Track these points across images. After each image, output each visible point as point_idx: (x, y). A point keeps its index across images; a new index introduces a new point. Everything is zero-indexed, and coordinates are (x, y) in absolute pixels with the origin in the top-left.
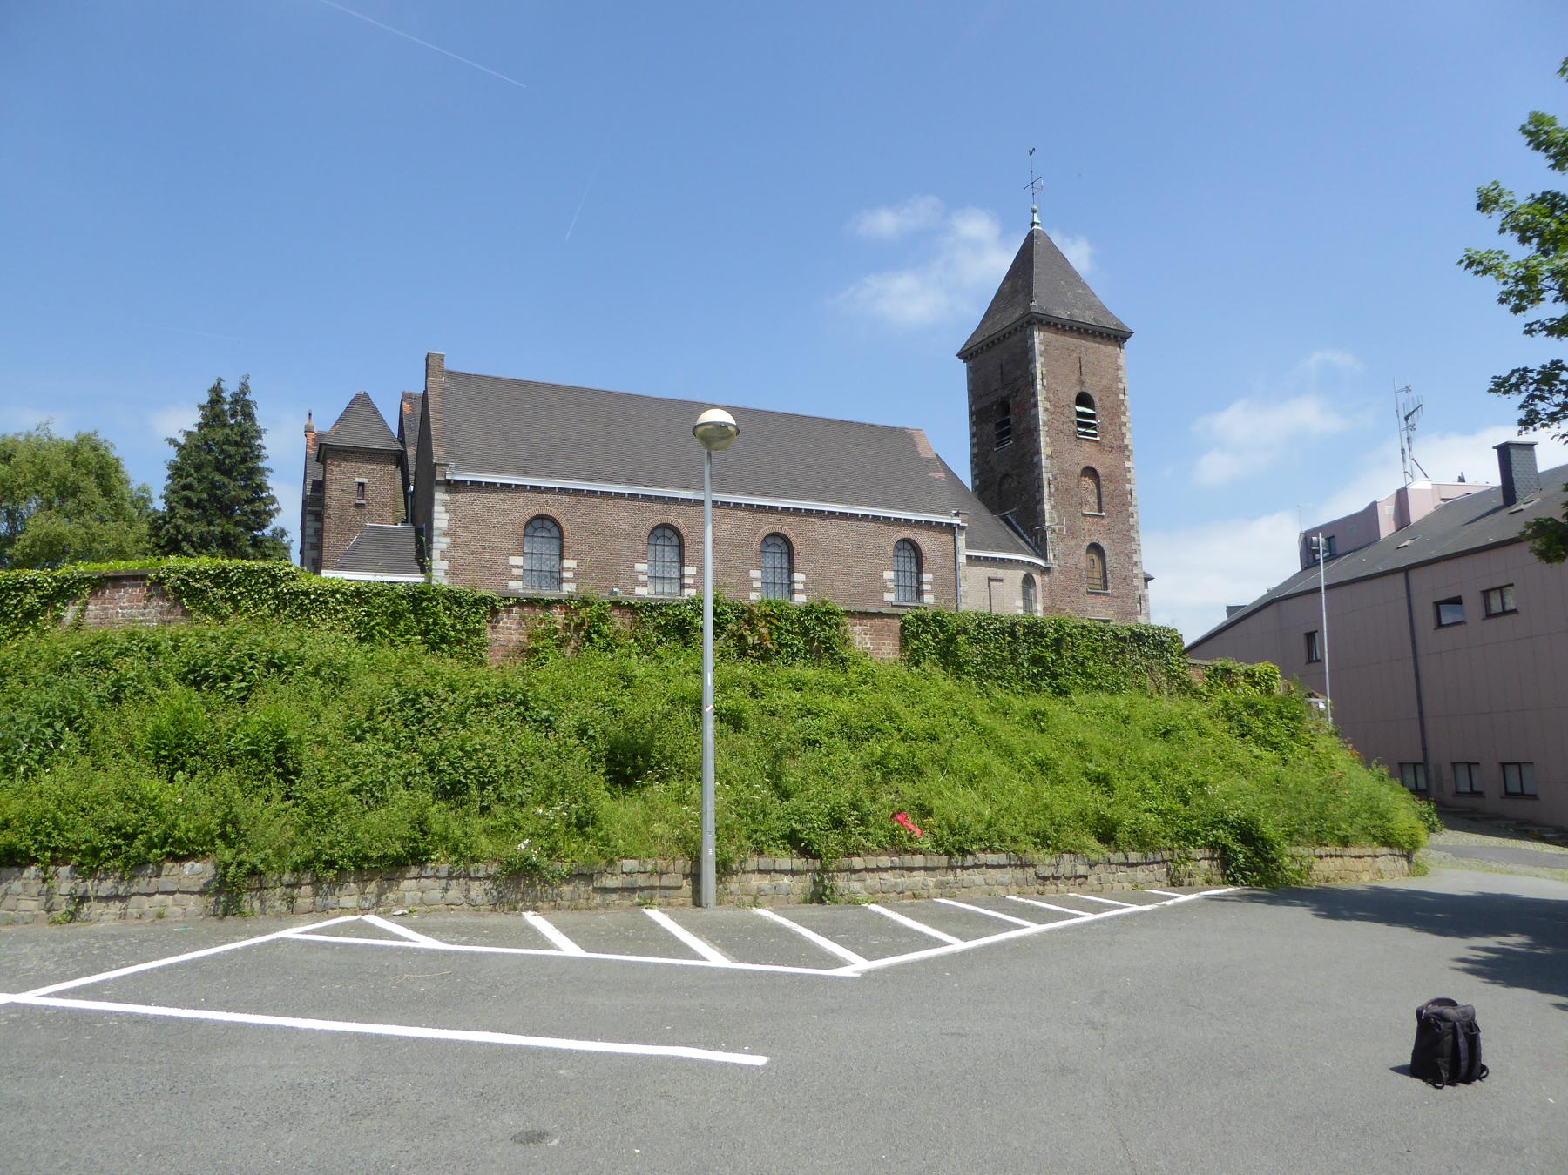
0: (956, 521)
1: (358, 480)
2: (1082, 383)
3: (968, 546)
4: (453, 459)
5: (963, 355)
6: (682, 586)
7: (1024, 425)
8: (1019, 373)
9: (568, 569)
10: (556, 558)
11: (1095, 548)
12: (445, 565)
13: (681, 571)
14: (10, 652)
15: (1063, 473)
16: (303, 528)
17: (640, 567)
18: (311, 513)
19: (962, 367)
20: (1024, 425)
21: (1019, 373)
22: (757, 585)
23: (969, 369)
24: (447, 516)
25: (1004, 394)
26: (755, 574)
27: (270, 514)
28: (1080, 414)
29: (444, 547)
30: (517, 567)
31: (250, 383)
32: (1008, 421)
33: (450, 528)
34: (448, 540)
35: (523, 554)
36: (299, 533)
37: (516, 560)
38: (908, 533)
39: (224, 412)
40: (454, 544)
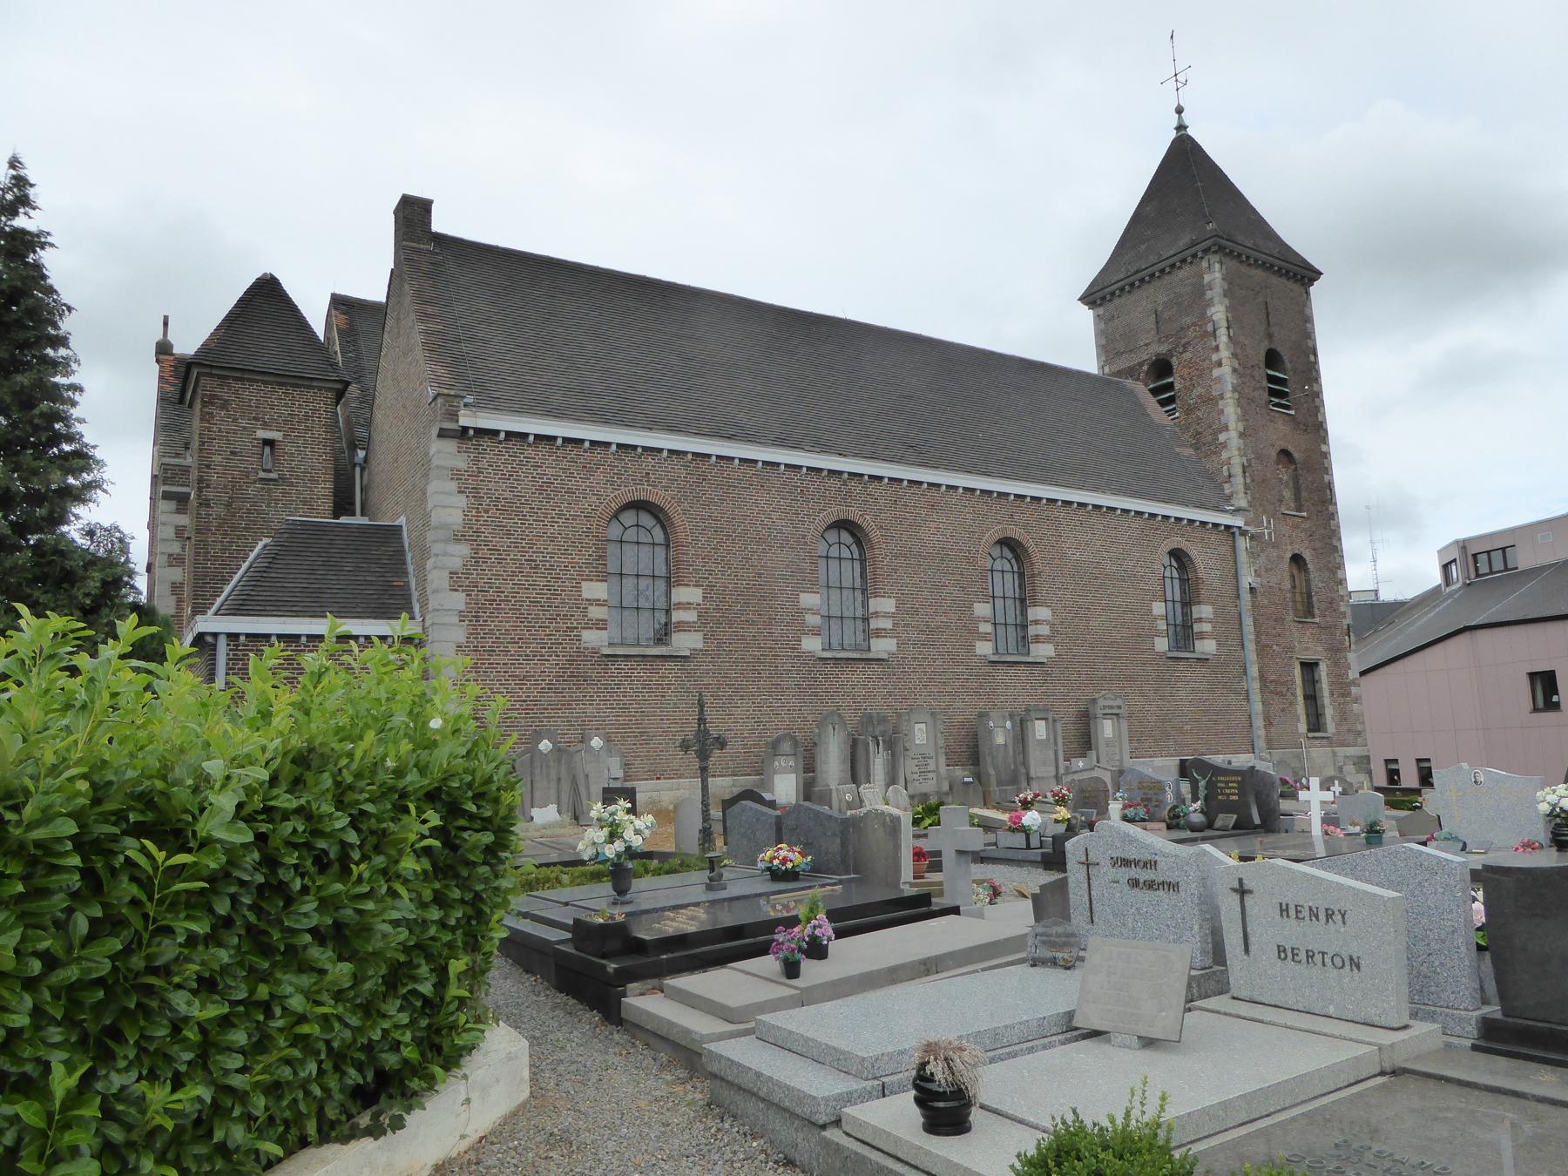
0: (1238, 521)
1: (262, 434)
2: (1270, 336)
3: (353, 514)
4: (468, 388)
5: (1094, 297)
6: (869, 634)
7: (1199, 390)
8: (1188, 320)
9: (686, 606)
10: (661, 585)
11: (1297, 559)
12: (459, 600)
13: (865, 604)
14: (8, 563)
15: (1259, 457)
16: (152, 526)
17: (809, 599)
18: (167, 496)
19: (1087, 315)
20: (1199, 390)
21: (1188, 320)
22: (986, 628)
23: (1098, 317)
24: (462, 501)
25: (1163, 349)
26: (982, 609)
27: (79, 495)
28: (1271, 379)
29: (456, 563)
30: (598, 603)
31: (30, 174)
32: (1170, 386)
33: (467, 524)
34: (464, 550)
35: (603, 577)
36: (147, 533)
37: (595, 590)
38: (1182, 543)
39: (405, 840)
40: (476, 559)
